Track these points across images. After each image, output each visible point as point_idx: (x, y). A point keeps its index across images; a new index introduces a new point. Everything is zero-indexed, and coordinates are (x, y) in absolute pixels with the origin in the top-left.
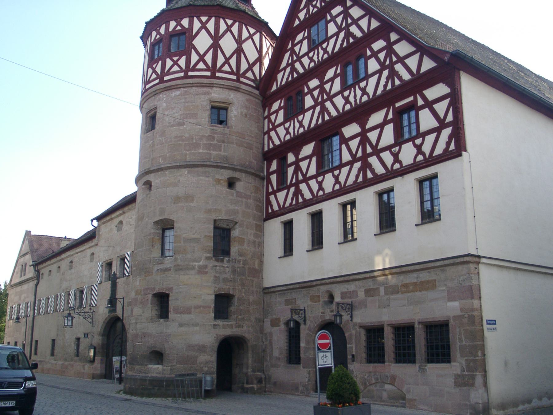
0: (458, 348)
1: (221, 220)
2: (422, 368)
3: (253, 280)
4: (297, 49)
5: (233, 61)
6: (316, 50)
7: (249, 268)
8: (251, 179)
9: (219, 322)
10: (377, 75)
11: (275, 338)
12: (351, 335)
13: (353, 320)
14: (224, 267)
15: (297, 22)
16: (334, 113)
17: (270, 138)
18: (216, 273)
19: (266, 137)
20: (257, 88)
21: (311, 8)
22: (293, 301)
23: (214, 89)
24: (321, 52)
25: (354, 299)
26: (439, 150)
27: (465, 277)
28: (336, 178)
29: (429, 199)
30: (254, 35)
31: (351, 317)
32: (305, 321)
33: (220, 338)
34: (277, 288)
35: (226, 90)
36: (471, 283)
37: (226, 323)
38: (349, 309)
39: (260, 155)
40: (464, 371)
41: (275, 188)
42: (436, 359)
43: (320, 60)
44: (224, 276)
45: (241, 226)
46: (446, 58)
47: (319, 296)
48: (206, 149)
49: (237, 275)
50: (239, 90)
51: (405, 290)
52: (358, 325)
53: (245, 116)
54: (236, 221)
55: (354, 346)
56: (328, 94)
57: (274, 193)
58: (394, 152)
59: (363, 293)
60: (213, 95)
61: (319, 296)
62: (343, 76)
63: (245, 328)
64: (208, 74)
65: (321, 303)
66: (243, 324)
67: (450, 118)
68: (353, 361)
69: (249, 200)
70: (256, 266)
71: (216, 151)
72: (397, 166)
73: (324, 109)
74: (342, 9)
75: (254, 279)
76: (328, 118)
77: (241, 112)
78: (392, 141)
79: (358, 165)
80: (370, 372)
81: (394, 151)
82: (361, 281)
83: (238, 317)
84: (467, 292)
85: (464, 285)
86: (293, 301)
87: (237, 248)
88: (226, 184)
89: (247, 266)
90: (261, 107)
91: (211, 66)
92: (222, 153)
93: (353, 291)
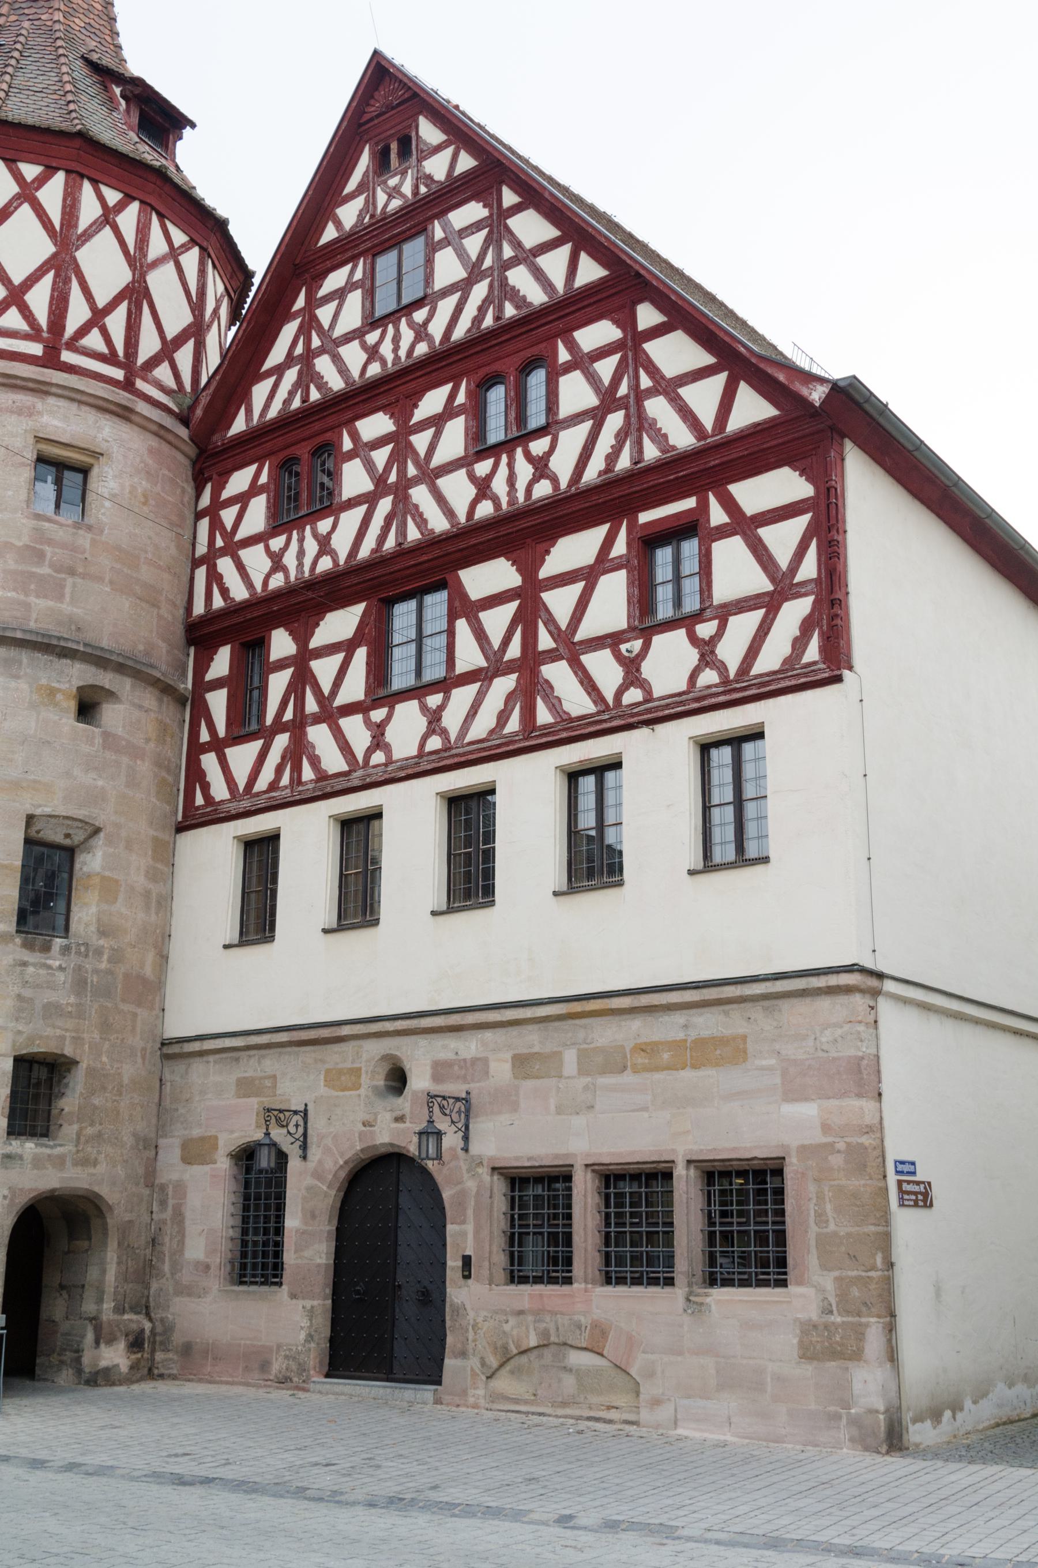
0: (813, 1243)
1: (50, 816)
3: (135, 1015)
4: (324, 314)
5: (116, 322)
6: (390, 326)
7: (126, 976)
8: (149, 698)
9: (29, 1147)
12: (463, 1194)
13: (471, 1148)
14: (49, 967)
15: (330, 233)
16: (439, 523)
17: (214, 577)
18: (24, 986)
19: (201, 573)
20: (184, 420)
21: (381, 197)
23: (51, 400)
26: (769, 660)
27: (839, 1032)
28: (434, 718)
29: (731, 800)
30: (183, 253)
31: (466, 1138)
32: (304, 1147)
34: (212, 1041)
35: (87, 408)
36: (859, 1049)
37: (48, 1151)
38: (459, 1112)
39: (179, 630)
40: (831, 1312)
41: (222, 731)
43: (403, 359)
45: (110, 842)
46: (817, 395)
47: (356, 1072)
48: (15, 589)
49: (89, 994)
50: (127, 414)
52: (485, 1163)
53: (142, 500)
54: (97, 824)
55: (470, 1228)
56: (423, 465)
57: (218, 746)
58: (627, 654)
59: (507, 1066)
60: (45, 419)
61: (356, 1072)
62: (477, 412)
63: (101, 1169)
64: (36, 349)
65: (362, 1091)
66: (99, 1152)
67: (809, 569)
68: (467, 1276)
69: (139, 762)
70: (148, 971)
71: (45, 597)
72: (633, 695)
73: (404, 508)
74: (485, 213)
75: (139, 1011)
76: (419, 536)
77: (132, 486)
78: (620, 622)
80: (521, 1313)
81: (627, 651)
82: (500, 1032)
84: (844, 1077)
85: (835, 1055)
86: (268, 1083)
87: (94, 909)
88: (72, 705)
89: (123, 970)
90: (190, 478)
92: (66, 607)
93: (475, 1061)
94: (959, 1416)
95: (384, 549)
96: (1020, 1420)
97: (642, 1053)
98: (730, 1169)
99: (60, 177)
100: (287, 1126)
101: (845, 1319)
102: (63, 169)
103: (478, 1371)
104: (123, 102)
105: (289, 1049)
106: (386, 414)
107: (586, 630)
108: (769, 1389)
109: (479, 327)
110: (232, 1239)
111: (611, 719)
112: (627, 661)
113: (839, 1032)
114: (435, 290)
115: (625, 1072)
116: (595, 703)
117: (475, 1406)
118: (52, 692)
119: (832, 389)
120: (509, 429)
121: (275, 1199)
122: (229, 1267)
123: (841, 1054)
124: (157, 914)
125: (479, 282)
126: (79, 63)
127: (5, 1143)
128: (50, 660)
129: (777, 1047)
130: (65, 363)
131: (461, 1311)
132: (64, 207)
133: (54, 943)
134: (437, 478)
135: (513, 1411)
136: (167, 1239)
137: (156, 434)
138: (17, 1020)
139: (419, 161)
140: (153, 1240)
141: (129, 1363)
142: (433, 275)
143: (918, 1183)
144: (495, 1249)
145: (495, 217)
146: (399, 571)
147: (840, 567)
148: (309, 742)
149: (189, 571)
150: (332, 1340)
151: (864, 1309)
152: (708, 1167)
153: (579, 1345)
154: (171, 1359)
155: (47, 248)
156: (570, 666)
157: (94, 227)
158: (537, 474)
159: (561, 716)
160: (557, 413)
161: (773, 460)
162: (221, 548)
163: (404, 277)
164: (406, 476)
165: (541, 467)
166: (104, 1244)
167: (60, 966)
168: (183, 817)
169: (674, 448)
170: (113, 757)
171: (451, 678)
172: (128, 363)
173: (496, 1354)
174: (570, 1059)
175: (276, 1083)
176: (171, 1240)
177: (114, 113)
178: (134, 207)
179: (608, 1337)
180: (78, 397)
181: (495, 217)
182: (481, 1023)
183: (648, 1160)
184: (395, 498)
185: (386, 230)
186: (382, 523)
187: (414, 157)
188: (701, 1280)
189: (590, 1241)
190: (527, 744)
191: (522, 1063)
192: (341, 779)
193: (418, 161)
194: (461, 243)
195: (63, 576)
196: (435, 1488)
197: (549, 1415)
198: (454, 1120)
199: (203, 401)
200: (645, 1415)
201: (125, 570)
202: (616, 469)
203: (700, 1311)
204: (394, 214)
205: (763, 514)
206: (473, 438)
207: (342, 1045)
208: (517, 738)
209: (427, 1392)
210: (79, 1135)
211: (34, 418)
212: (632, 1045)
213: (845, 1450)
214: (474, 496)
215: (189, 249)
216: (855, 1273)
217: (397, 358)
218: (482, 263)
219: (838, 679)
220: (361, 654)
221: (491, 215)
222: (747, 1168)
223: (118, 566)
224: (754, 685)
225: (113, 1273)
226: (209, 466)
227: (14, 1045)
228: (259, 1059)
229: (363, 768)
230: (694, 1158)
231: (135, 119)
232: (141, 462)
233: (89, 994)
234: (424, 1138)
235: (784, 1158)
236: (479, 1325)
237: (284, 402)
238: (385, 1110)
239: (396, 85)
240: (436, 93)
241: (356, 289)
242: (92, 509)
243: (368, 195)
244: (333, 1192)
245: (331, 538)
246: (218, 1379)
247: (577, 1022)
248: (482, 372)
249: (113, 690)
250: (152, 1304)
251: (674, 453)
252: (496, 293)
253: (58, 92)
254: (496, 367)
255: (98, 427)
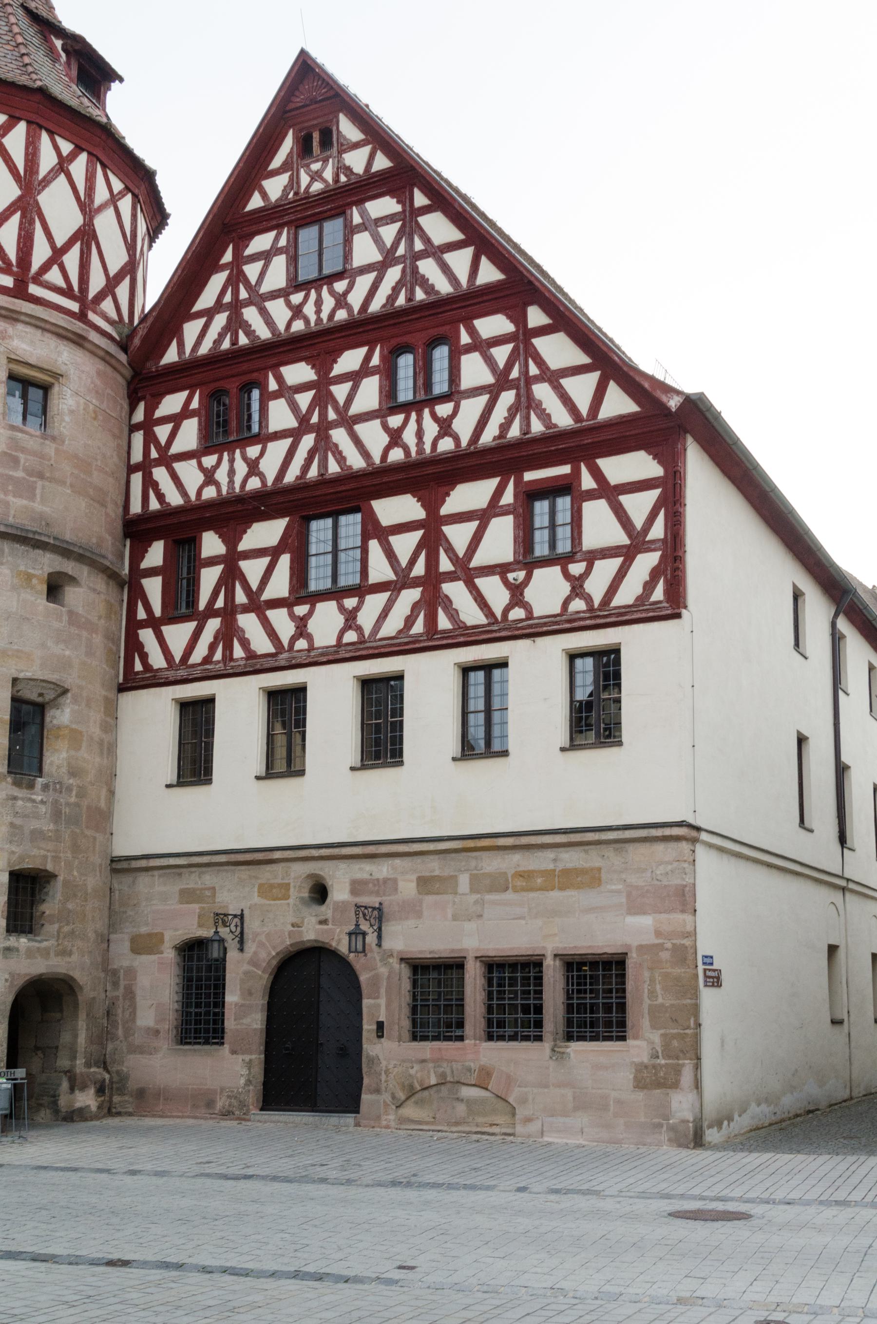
0: (646, 1011)
2: (560, 1052)
3: (95, 838)
5: (72, 260)
6: (313, 291)
7: (89, 808)
8: (100, 583)
9: (23, 942)
10: (485, 398)
11: (143, 982)
14: (34, 801)
17: (149, 483)
18: (15, 816)
19: (137, 479)
21: (305, 179)
22: (208, 893)
23: (20, 327)
24: (329, 303)
25: (388, 898)
26: (626, 596)
27: (669, 867)
30: (120, 199)
31: (380, 937)
32: (242, 942)
33: (20, 983)
36: (684, 879)
37: (36, 944)
40: (658, 1057)
41: (158, 612)
42: (590, 1032)
43: (325, 321)
44: (35, 824)
45: (75, 701)
46: (673, 403)
49: (63, 822)
50: (81, 341)
51: (524, 884)
52: (395, 955)
53: (93, 415)
54: (66, 686)
55: (382, 1002)
56: (342, 411)
58: (513, 581)
59: (413, 885)
63: (75, 958)
65: (291, 901)
66: (73, 946)
67: (658, 531)
69: (94, 636)
70: (103, 804)
71: (21, 496)
72: (518, 613)
74: (398, 208)
75: (98, 835)
79: (411, 595)
80: (423, 1061)
83: (62, 930)
85: (667, 883)
87: (64, 755)
89: (86, 803)
90: (126, 396)
91: (14, 262)
92: (37, 506)
93: (386, 881)
94: (732, 1124)
95: (308, 477)
96: (762, 1128)
97: (521, 878)
98: (585, 960)
99: (22, 127)
100: (229, 926)
101: (667, 1061)
102: (25, 120)
103: (389, 1102)
104: (63, 55)
105: (226, 868)
106: (308, 365)
107: (479, 559)
108: (612, 1108)
109: (393, 305)
110: (177, 1011)
111: (499, 630)
112: (513, 587)
113: (669, 867)
114: (354, 267)
115: (508, 892)
116: (486, 616)
117: (387, 1127)
118: (29, 577)
119: (685, 399)
120: (418, 392)
121: (214, 981)
122: (175, 1032)
123: (671, 883)
124: (108, 758)
125: (393, 266)
126: (20, 11)
127: (5, 939)
128: (27, 551)
129: (624, 876)
130: (32, 295)
131: (375, 1061)
132: (27, 154)
133: (37, 782)
134: (355, 424)
135: (417, 1130)
136: (120, 1011)
137: (103, 359)
138: (10, 842)
139: (340, 152)
140: (108, 1012)
141: (97, 1104)
142: (351, 253)
143: (714, 970)
144: (403, 1016)
145: (408, 214)
146: (321, 495)
147: (681, 533)
148: (239, 627)
149: (125, 475)
150: (265, 1084)
151: (681, 1055)
152: (570, 960)
153: (470, 1083)
154: (126, 1101)
155: (13, 192)
156: (467, 586)
157: (52, 174)
158: (442, 432)
159: (458, 624)
160: (459, 385)
161: (633, 444)
162: (155, 459)
163: (325, 250)
164: (327, 418)
165: (445, 427)
166: (75, 1016)
167: (42, 800)
168: (124, 680)
169: (555, 426)
170: (76, 632)
171: (364, 586)
172: (81, 297)
173: (404, 1090)
174: (464, 881)
175: (215, 893)
176: (123, 1012)
177: (56, 65)
178: (83, 157)
179: (491, 1077)
180: (42, 325)
181: (408, 214)
182: (392, 853)
183: (525, 954)
184: (317, 436)
185: (309, 207)
186: (306, 455)
187: (335, 149)
188: (562, 1036)
189: (478, 1011)
190: (430, 644)
191: (425, 884)
192: (270, 659)
193: (339, 152)
194: (377, 230)
195: (35, 479)
196: (414, 1175)
197: (446, 1132)
198: (373, 924)
199: (141, 332)
200: (519, 1129)
201: (82, 475)
202: (508, 437)
203: (562, 1058)
204: (315, 196)
205: (623, 485)
206: (386, 396)
207: (273, 865)
208: (422, 638)
209: (349, 1119)
210: (58, 932)
211: (7, 341)
212: (513, 871)
213: (665, 1147)
214: (387, 443)
215: (124, 196)
216: (675, 1031)
217: (319, 320)
218: (396, 250)
219: (678, 616)
220: (285, 560)
221: (404, 211)
222: (598, 960)
223: (76, 472)
224: (614, 614)
225: (83, 1036)
226: (143, 387)
227: (9, 863)
228: (199, 874)
229: (288, 651)
230: (560, 953)
231: (74, 73)
232: (92, 383)
233: (63, 822)
234: (353, 937)
235: (626, 954)
236: (390, 1071)
237: (215, 342)
238: (311, 915)
239: (320, 83)
240: (381, 120)
241: (281, 253)
242: (54, 423)
243: (292, 174)
244: (266, 976)
245: (259, 463)
246: (169, 1114)
247: (469, 854)
248: (394, 342)
249: (75, 576)
250: (108, 1060)
251: (556, 430)
252: (408, 278)
253: (11, 43)
254: (407, 339)
255: (59, 352)
